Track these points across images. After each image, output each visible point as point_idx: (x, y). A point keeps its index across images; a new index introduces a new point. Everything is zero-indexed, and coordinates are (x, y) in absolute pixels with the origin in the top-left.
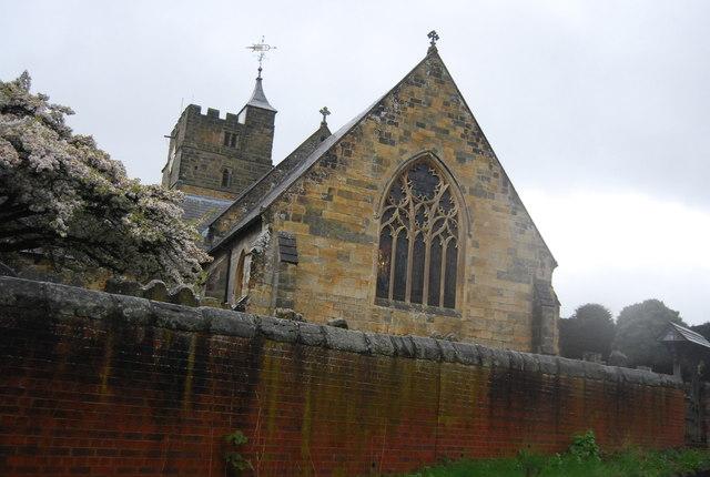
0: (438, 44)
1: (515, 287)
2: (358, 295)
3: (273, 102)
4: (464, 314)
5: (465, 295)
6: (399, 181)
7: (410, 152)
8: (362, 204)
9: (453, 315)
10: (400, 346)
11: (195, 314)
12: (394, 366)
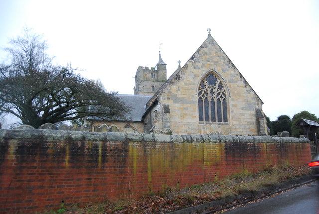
0: (211, 33)
1: (249, 112)
2: (193, 122)
3: (165, 61)
4: (231, 124)
5: (231, 117)
6: (203, 81)
7: (204, 71)
8: (191, 91)
9: (227, 124)
10: (185, 139)
11: (100, 135)
12: (184, 146)
